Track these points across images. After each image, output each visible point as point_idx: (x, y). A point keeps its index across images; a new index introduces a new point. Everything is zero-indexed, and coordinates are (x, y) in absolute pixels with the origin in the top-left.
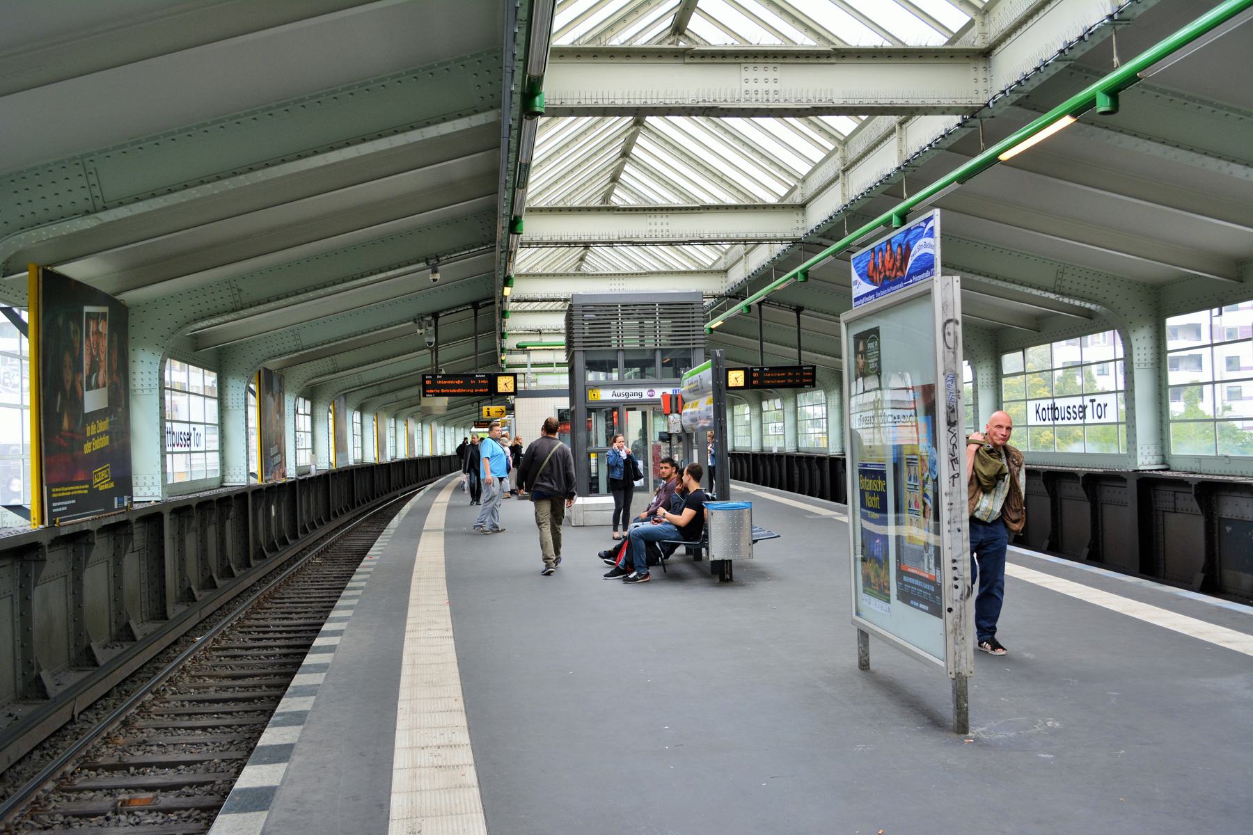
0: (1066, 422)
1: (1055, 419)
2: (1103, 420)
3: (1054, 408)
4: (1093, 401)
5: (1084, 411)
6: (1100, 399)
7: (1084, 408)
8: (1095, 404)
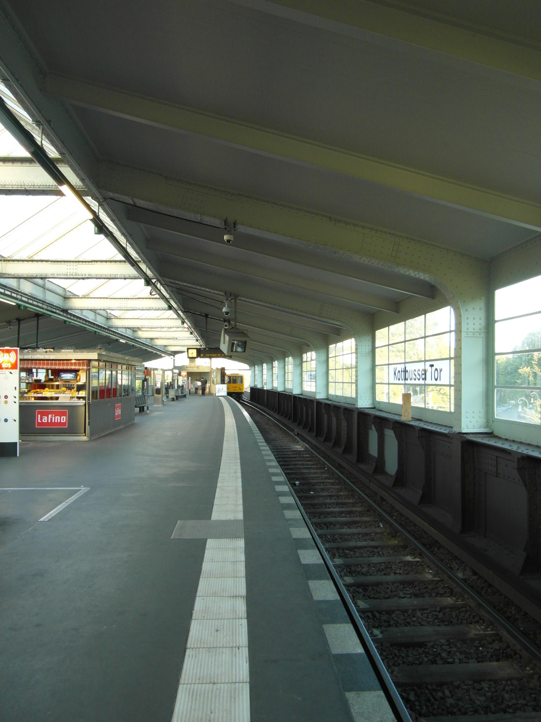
0: (413, 382)
1: (406, 379)
2: (438, 382)
3: (405, 371)
4: (432, 366)
5: (425, 374)
6: (437, 365)
7: (425, 371)
8: (434, 368)
